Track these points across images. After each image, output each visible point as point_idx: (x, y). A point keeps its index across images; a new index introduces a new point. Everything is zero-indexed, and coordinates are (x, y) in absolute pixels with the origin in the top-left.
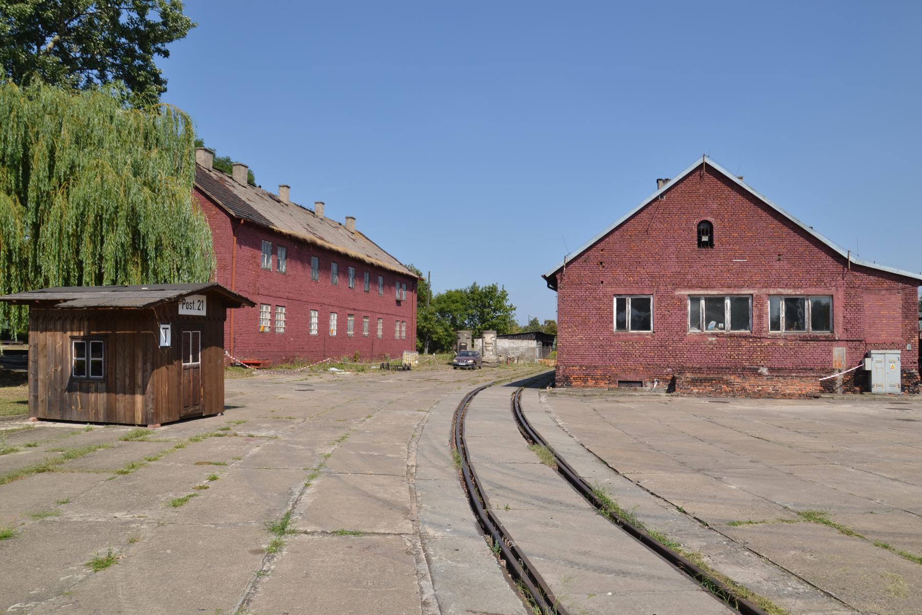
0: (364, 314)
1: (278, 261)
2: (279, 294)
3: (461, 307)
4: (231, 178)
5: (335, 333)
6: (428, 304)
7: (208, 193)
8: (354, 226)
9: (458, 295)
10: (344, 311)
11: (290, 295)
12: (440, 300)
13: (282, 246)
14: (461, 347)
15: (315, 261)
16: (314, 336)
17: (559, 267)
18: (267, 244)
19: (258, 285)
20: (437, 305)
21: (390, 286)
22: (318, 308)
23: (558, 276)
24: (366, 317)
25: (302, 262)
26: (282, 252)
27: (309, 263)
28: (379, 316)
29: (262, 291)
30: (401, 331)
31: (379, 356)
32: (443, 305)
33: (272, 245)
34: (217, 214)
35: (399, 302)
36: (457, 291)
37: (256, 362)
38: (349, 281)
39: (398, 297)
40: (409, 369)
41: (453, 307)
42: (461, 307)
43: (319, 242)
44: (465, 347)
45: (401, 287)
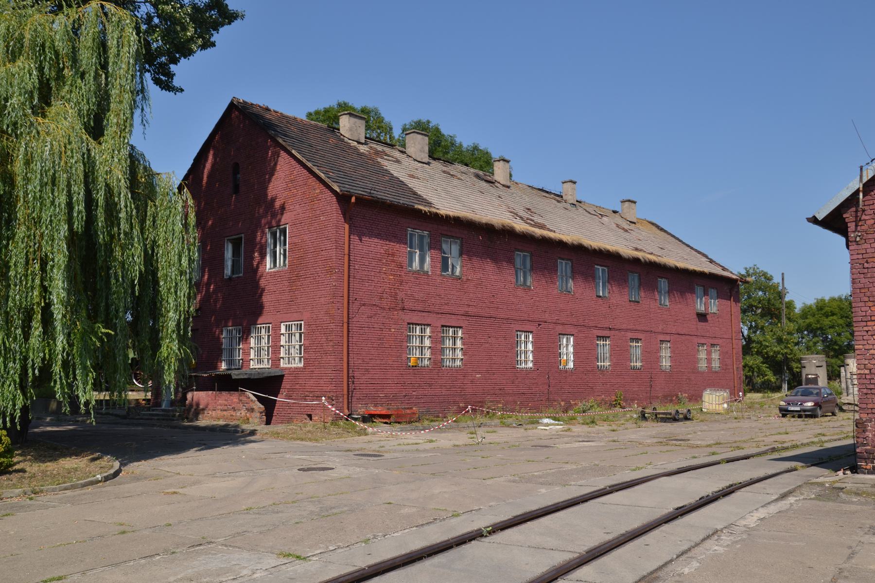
0: (630, 335)
1: (445, 261)
2: (446, 309)
3: (841, 321)
4: (403, 152)
5: (571, 365)
6: (784, 320)
7: (309, 164)
8: (633, 213)
9: (835, 304)
10: (587, 335)
11: (471, 310)
12: (806, 312)
13: (662, 278)
14: (809, 381)
15: (564, 266)
16: (528, 371)
17: (846, 194)
18: (417, 234)
19: (401, 295)
20: (801, 321)
21: (682, 293)
22: (532, 328)
23: (849, 216)
24: (637, 340)
25: (495, 260)
26: (452, 249)
27: (511, 261)
28: (662, 337)
29: (408, 304)
30: (708, 359)
31: (665, 397)
32: (810, 320)
33: (430, 236)
34: (321, 193)
35: (702, 317)
36: (833, 300)
37: (384, 412)
38: (596, 287)
39: (700, 308)
40: (686, 418)
41: (826, 322)
42: (841, 321)
43: (538, 232)
44: (815, 381)
45: (706, 293)
